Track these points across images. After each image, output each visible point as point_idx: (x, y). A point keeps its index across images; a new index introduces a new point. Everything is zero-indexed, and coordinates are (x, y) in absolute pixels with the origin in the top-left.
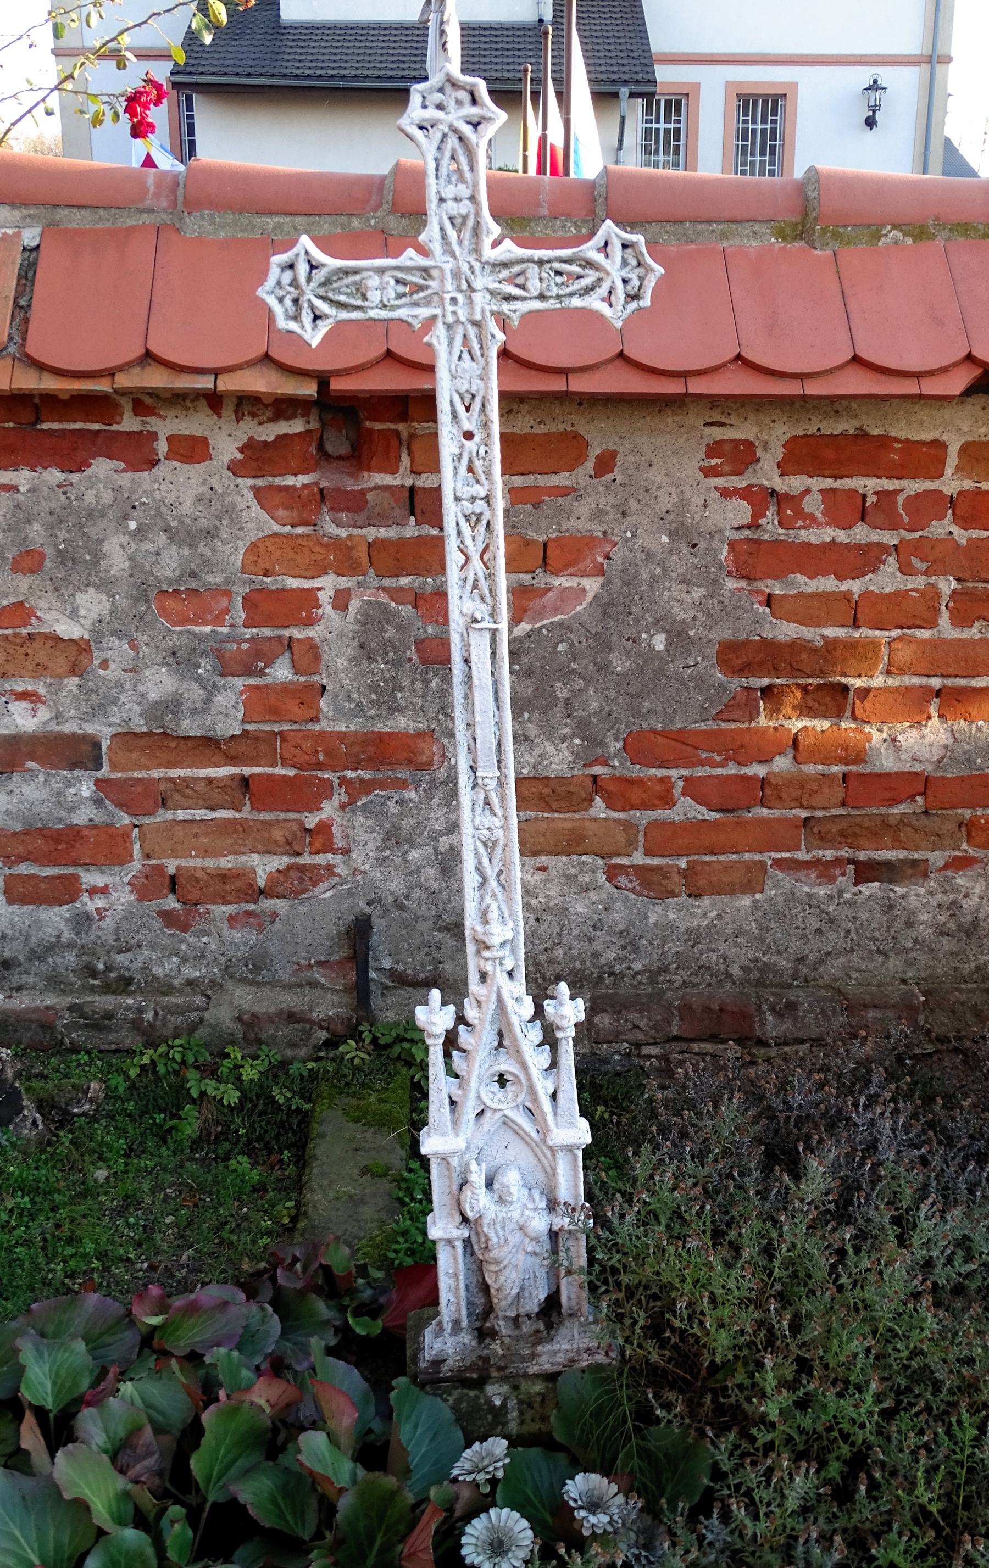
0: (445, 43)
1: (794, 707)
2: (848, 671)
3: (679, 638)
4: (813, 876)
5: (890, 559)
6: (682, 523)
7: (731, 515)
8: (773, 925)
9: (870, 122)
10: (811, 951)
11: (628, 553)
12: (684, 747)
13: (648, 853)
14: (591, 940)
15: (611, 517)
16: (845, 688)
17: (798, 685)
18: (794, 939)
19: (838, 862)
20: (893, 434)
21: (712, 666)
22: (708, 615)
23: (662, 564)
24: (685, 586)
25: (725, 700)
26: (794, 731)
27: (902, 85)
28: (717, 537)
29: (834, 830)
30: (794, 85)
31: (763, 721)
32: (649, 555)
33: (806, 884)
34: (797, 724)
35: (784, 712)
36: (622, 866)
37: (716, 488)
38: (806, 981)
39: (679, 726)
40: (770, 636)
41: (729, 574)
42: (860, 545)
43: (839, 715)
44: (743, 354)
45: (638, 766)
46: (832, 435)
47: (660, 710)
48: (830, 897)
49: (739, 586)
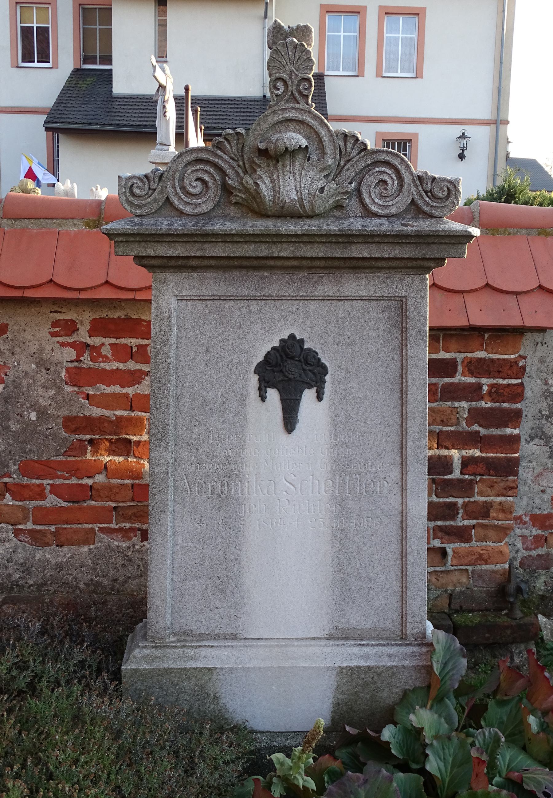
0: (165, 112)
1: (106, 450)
2: (129, 432)
3: (42, 413)
4: (120, 537)
5: (146, 378)
6: (42, 358)
7: (66, 355)
8: (100, 562)
9: (461, 157)
10: (120, 576)
11: (16, 373)
12: (49, 469)
13: (34, 523)
14: (7, 567)
15: (6, 355)
16: (129, 441)
17: (107, 439)
18: (111, 569)
19: (132, 529)
20: (143, 318)
21: (60, 428)
22: (57, 403)
23: (33, 378)
24: (44, 389)
25: (68, 445)
26: (105, 462)
27: (480, 136)
28: (59, 365)
29: (130, 513)
30: (416, 135)
31: (89, 456)
32: (26, 374)
33: (117, 541)
34: (106, 459)
35: (100, 452)
36: (21, 529)
37: (58, 342)
38: (118, 591)
39: (45, 458)
40: (88, 414)
41: (67, 383)
42: (130, 370)
43: (128, 455)
44: (53, 279)
45: (26, 478)
46: (113, 318)
47: (35, 450)
48: (129, 548)
49: (73, 390)
